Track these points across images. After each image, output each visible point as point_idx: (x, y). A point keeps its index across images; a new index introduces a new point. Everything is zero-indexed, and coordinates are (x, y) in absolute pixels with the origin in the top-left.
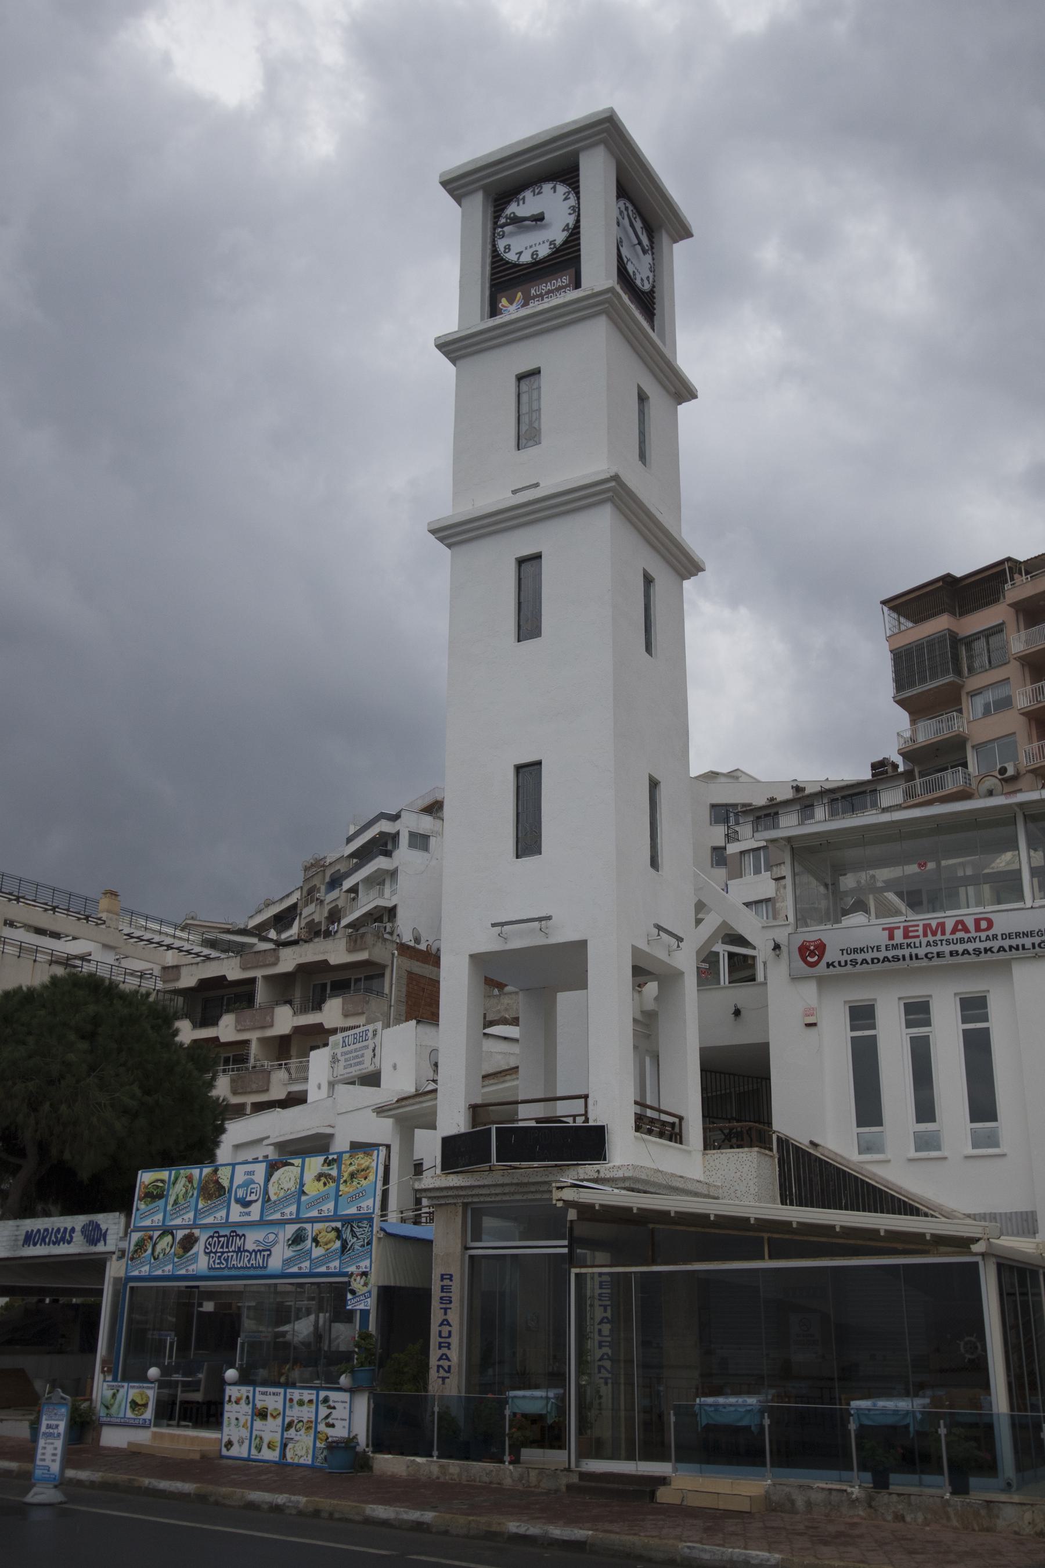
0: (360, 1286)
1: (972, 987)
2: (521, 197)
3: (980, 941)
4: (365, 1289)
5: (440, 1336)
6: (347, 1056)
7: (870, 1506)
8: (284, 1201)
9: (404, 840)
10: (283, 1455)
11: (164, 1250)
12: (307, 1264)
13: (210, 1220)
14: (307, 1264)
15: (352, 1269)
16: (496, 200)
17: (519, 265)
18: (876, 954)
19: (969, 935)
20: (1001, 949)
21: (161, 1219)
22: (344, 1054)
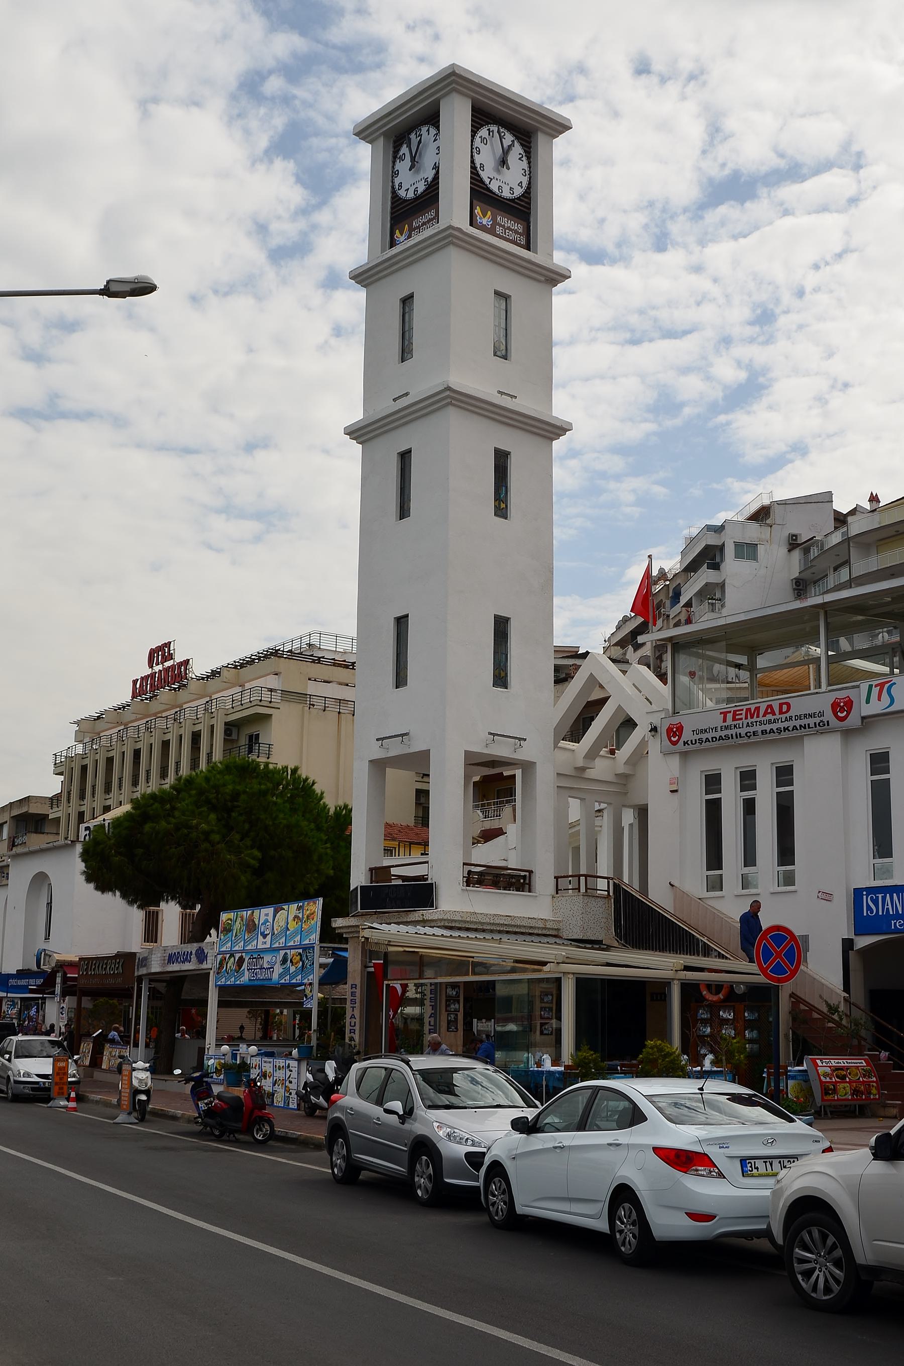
1: (782, 757)
4: (311, 994)
5: (351, 1026)
9: (730, 551)
15: (306, 981)
16: (395, 142)
18: (714, 734)
19: (775, 717)
20: (795, 728)
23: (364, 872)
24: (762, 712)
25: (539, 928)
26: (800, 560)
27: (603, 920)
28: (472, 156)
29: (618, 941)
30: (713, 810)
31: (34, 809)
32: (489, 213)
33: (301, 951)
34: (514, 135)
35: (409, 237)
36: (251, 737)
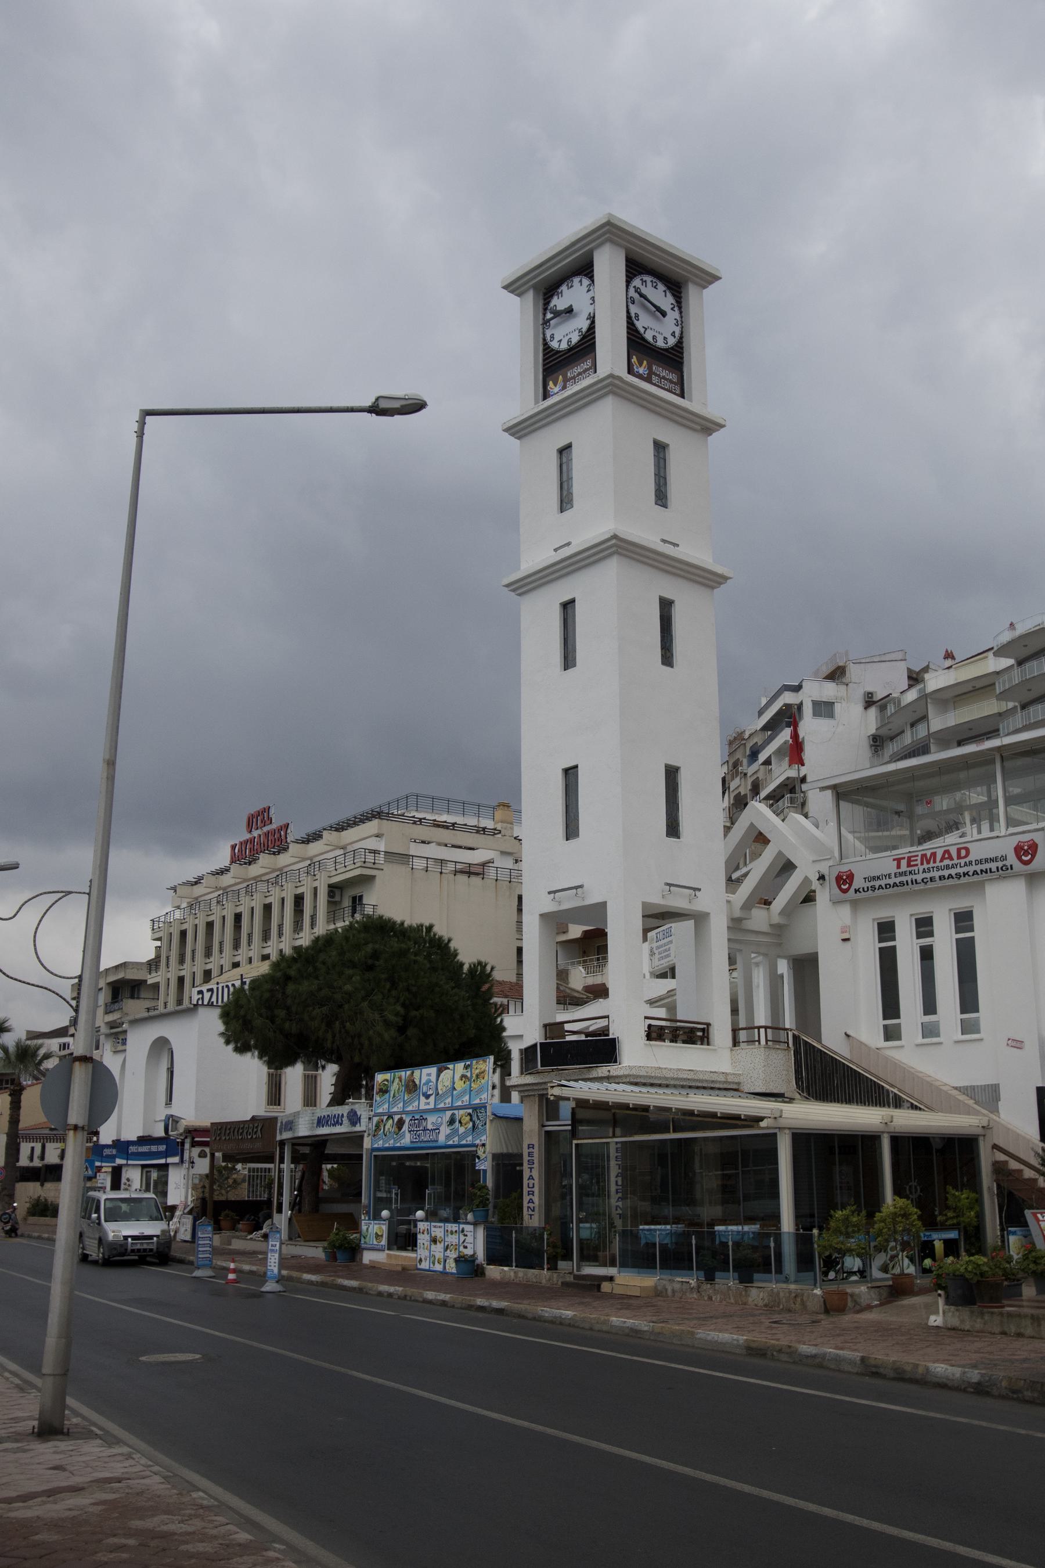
0: (481, 1153)
1: (961, 904)
2: (560, 291)
3: (961, 867)
4: (484, 1156)
6: (660, 950)
7: (699, 1292)
8: (445, 1094)
9: (808, 710)
10: (445, 1267)
11: (389, 1129)
12: (456, 1139)
13: (410, 1108)
14: (456, 1139)
15: (477, 1142)
16: (545, 294)
17: (560, 352)
18: (888, 881)
19: (953, 862)
20: (975, 873)
21: (468, 1100)
22: (658, 948)
23: (538, 1029)
24: (939, 858)
25: (720, 1082)
26: (876, 718)
27: (784, 1072)
28: (627, 306)
29: (800, 1094)
30: (888, 961)
31: (132, 975)
32: (645, 362)
33: (470, 1111)
34: (666, 285)
35: (564, 388)
36: (354, 899)
